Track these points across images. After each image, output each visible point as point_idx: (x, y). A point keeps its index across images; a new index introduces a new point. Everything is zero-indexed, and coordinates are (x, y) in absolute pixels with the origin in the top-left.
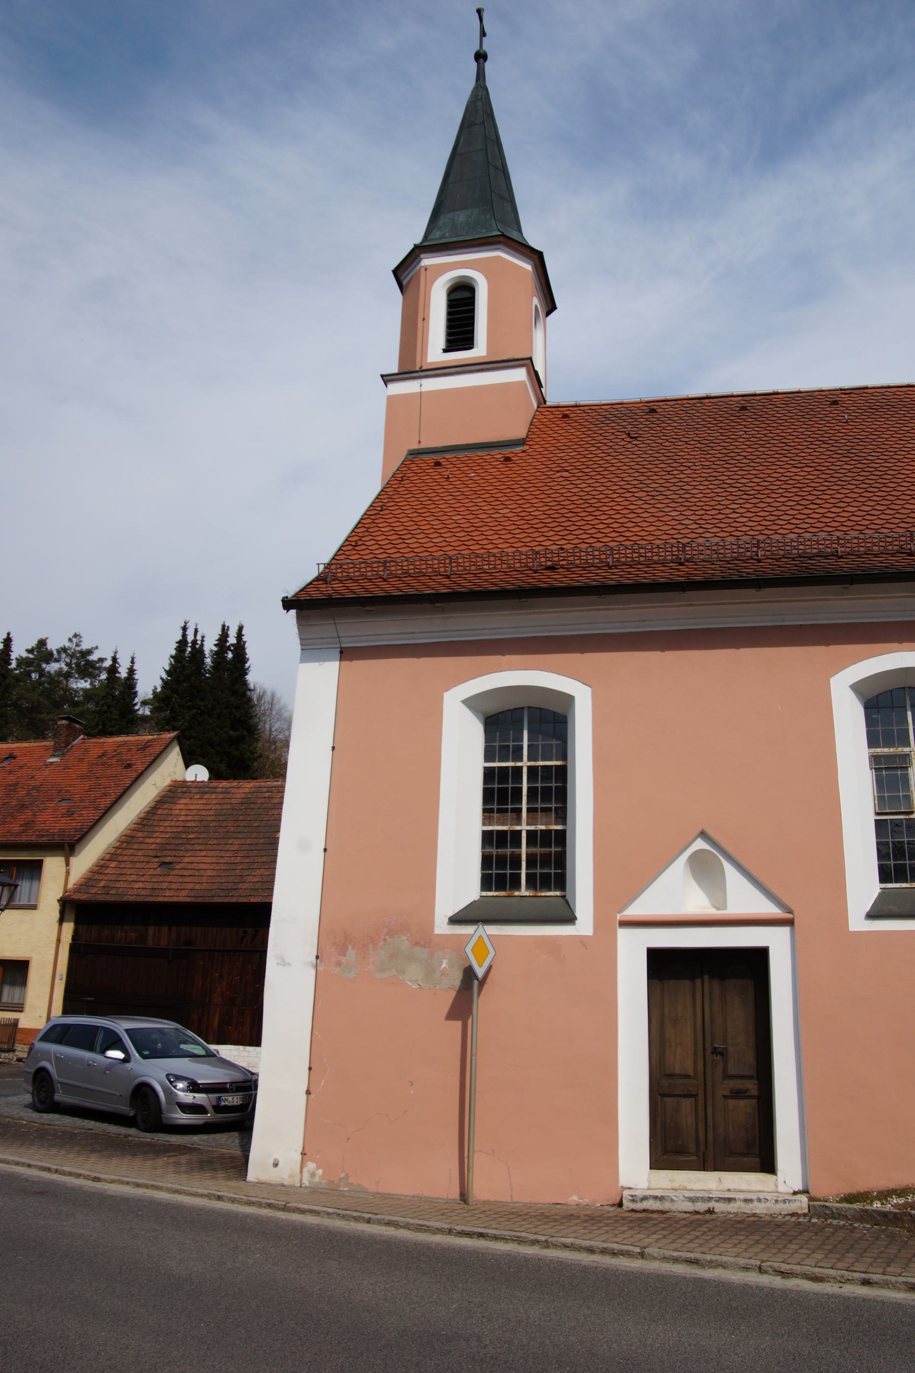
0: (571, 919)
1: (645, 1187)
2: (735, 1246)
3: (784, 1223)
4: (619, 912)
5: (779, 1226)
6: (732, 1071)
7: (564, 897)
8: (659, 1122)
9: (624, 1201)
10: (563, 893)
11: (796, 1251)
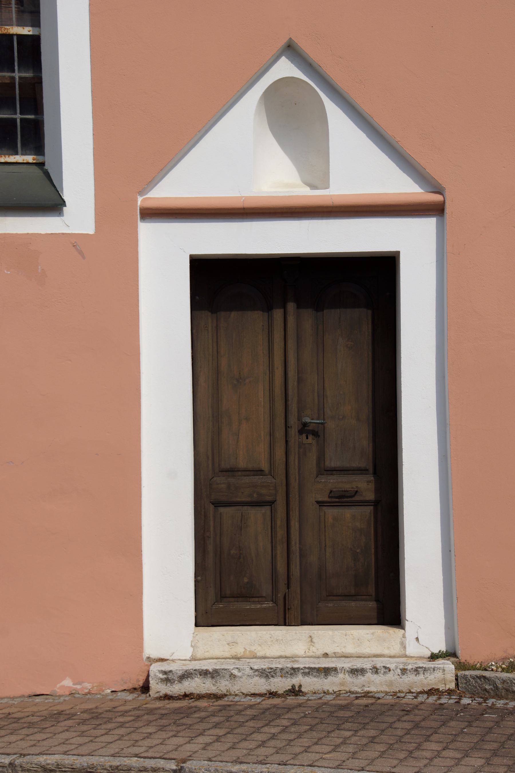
0: (54, 205)
1: (188, 656)
2: (336, 748)
3: (416, 707)
4: (141, 193)
5: (408, 712)
6: (332, 462)
7: (41, 165)
8: (210, 548)
9: (152, 683)
10: (40, 159)
11: (438, 754)
